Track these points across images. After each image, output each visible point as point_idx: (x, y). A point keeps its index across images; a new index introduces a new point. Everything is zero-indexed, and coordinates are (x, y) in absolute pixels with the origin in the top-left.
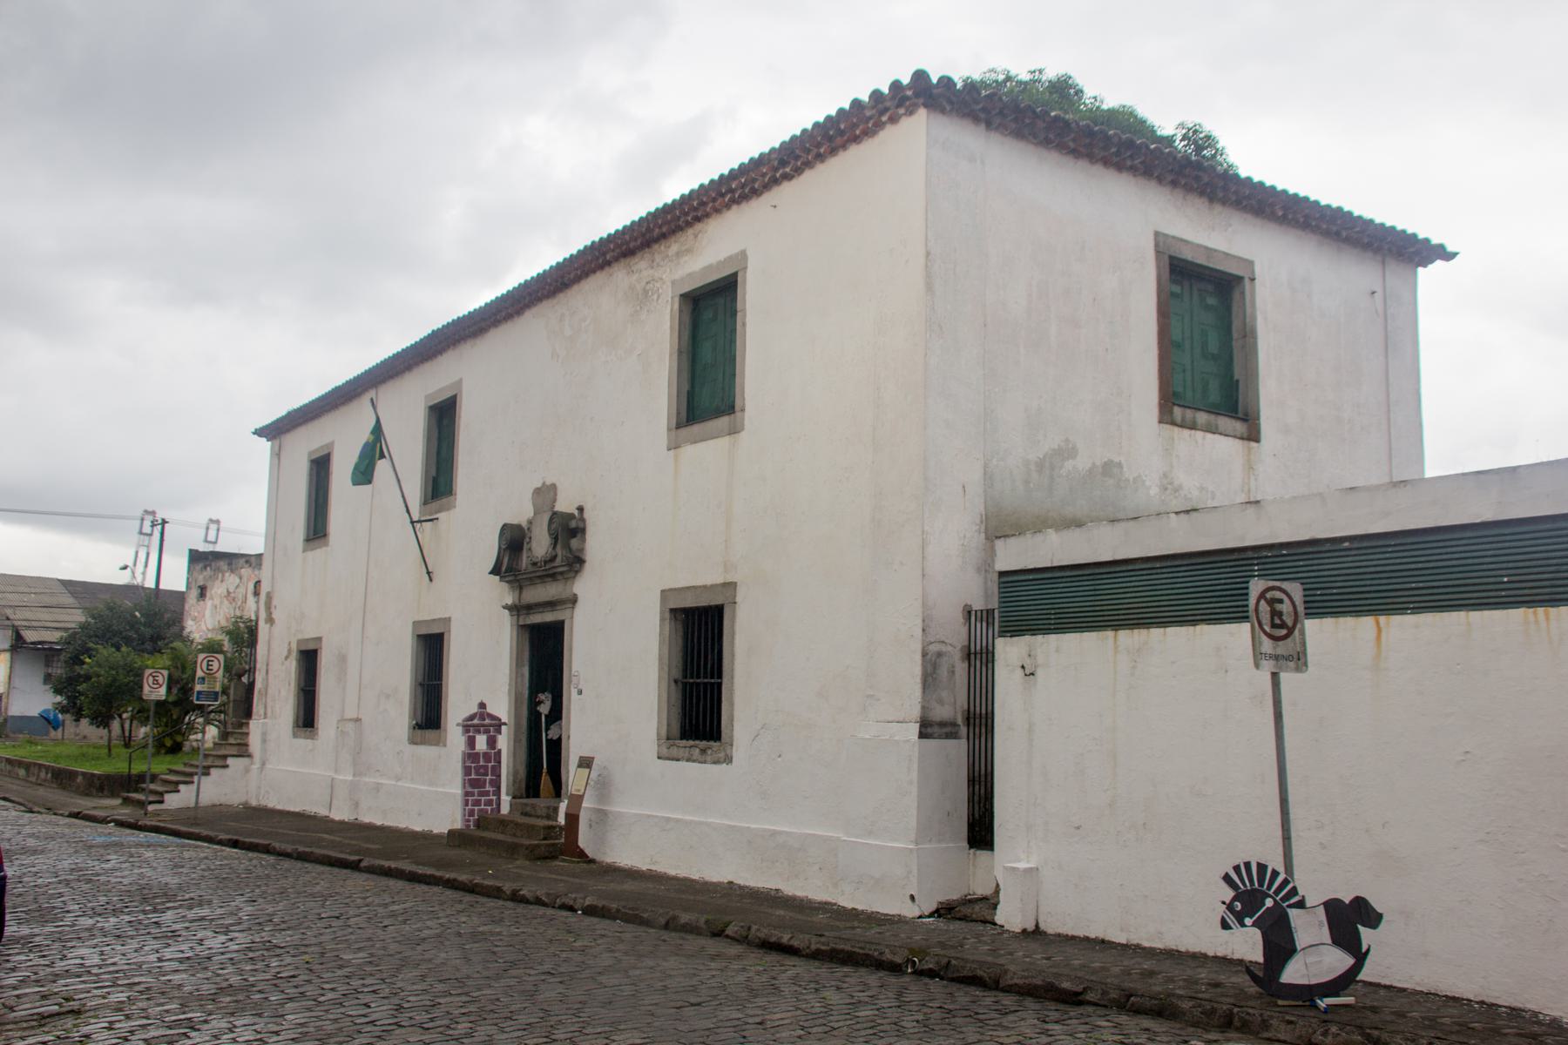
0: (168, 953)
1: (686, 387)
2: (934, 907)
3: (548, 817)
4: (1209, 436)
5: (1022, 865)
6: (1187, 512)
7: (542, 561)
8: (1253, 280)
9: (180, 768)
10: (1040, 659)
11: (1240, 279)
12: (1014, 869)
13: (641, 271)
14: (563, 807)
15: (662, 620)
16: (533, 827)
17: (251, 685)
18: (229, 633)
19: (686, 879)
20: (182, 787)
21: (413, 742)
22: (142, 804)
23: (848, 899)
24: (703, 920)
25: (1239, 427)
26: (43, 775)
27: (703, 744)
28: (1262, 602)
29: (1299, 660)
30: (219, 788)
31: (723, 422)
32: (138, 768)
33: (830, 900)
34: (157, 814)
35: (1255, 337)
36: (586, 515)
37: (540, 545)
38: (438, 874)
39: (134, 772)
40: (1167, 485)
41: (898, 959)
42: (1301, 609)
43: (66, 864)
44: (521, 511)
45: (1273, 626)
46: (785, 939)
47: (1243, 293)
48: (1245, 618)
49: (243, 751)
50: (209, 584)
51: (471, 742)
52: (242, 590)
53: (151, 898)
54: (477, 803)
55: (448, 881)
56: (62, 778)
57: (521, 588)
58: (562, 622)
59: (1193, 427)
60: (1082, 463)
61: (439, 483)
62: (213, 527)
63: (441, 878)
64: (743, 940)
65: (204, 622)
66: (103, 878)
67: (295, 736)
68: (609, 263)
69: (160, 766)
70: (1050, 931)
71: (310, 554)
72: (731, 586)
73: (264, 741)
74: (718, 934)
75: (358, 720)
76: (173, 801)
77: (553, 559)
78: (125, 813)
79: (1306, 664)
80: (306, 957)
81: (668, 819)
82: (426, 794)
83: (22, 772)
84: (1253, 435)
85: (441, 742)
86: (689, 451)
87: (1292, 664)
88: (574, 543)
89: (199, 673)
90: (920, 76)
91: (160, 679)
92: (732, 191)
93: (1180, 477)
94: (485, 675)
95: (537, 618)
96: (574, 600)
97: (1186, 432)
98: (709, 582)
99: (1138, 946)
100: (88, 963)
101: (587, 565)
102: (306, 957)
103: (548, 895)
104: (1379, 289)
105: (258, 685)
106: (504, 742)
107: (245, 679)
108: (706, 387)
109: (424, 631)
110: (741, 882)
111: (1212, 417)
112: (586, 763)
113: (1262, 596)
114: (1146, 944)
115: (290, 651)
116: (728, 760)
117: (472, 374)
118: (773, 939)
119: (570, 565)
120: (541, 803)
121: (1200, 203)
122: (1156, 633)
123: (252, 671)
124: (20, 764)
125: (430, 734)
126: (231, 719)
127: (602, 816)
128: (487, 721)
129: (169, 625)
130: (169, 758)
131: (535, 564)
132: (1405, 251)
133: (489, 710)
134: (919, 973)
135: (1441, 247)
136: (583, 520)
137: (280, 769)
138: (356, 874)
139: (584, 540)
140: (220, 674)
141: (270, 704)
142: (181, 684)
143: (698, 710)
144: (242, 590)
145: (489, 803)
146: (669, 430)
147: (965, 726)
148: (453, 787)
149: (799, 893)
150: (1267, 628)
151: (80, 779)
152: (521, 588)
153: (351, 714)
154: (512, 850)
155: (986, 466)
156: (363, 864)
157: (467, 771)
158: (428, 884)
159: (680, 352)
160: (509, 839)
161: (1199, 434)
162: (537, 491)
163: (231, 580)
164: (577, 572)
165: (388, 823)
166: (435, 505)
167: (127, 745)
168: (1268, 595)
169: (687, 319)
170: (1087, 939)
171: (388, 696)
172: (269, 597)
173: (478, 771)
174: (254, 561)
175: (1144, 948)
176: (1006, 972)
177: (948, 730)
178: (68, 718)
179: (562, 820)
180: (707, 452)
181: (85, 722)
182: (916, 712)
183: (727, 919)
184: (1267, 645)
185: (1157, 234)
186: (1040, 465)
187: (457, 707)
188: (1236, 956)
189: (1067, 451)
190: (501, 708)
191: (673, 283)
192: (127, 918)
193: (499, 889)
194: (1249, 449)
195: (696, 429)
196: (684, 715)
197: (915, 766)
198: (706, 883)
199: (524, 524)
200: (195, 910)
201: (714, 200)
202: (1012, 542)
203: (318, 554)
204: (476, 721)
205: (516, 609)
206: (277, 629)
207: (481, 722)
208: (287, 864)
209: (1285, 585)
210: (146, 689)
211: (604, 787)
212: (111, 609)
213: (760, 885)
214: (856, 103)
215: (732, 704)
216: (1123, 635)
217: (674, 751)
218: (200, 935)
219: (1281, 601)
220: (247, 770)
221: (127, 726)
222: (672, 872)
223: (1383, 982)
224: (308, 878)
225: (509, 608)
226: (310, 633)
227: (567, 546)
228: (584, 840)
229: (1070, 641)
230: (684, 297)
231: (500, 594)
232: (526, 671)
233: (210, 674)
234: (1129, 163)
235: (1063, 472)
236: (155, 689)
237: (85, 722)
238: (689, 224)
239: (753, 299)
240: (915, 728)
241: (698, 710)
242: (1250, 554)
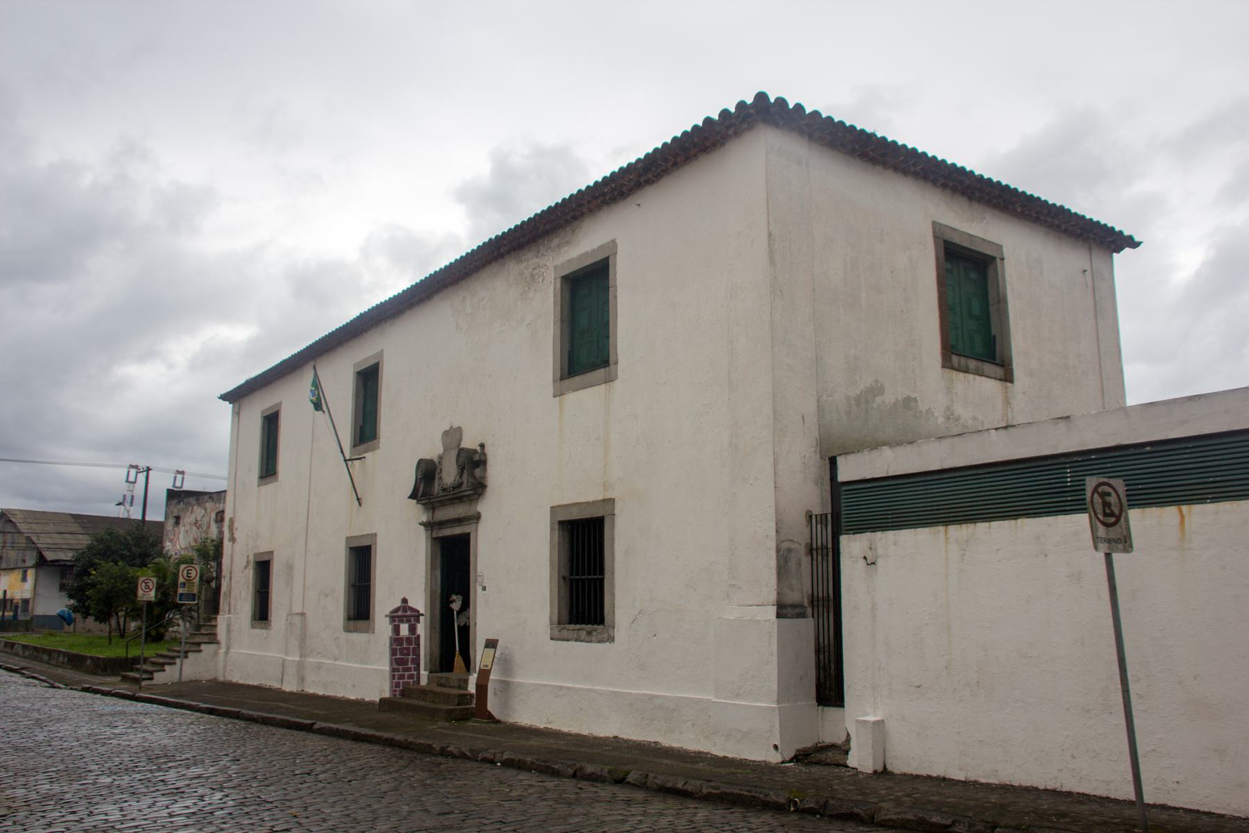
0: (176, 808)
1: (567, 348)
2: (792, 754)
3: (460, 687)
4: (978, 377)
5: (871, 718)
6: (1005, 428)
7: (452, 489)
8: (1003, 259)
9: (165, 652)
10: (880, 551)
11: (993, 259)
12: (865, 722)
13: (529, 262)
14: (473, 679)
15: (552, 530)
16: (449, 695)
17: (219, 587)
18: (198, 550)
19: (578, 736)
20: (167, 667)
21: (347, 630)
22: (136, 681)
23: (719, 749)
24: (606, 770)
25: (999, 371)
26: (61, 659)
28: (1096, 495)
29: (1125, 542)
30: (195, 667)
31: (601, 373)
32: (134, 652)
33: (702, 749)
34: (148, 688)
35: (1006, 302)
36: (487, 450)
37: (449, 475)
38: (378, 734)
39: (130, 656)
40: (950, 416)
41: (782, 801)
42: (1124, 500)
43: (84, 731)
44: (433, 449)
45: (1105, 515)
46: (680, 785)
48: (1084, 510)
49: (213, 639)
50: (182, 515)
51: (396, 630)
52: (206, 519)
53: (160, 758)
54: (402, 677)
55: (387, 740)
56: (76, 661)
58: (469, 534)
59: (966, 371)
60: (889, 398)
61: (366, 430)
62: (179, 477)
63: (348, 732)
64: (641, 786)
65: (179, 543)
66: (115, 742)
67: (253, 627)
69: (150, 651)
70: (896, 771)
71: (264, 488)
72: (610, 502)
73: (229, 631)
74: (620, 781)
75: (303, 614)
76: (159, 678)
77: (461, 485)
78: (124, 688)
79: (1131, 546)
80: (292, 811)
81: (561, 688)
82: (361, 670)
83: (45, 657)
84: (1008, 378)
85: (369, 630)
86: (572, 398)
87: (1121, 546)
88: (478, 472)
89: (181, 580)
90: (761, 97)
91: (150, 585)
92: (604, 194)
93: (960, 410)
94: (405, 576)
95: (448, 532)
96: (478, 517)
97: (962, 375)
98: (591, 499)
99: (975, 783)
100: (111, 818)
101: (489, 491)
102: (292, 811)
103: (471, 751)
104: (1087, 267)
105: (224, 589)
106: (421, 629)
107: (213, 584)
108: (586, 345)
109: (354, 544)
110: (625, 737)
111: (980, 364)
112: (491, 644)
113: (1095, 490)
114: (983, 780)
115: (248, 562)
116: (611, 639)
118: (669, 785)
120: (454, 676)
121: (963, 201)
122: (982, 527)
123: (219, 578)
124: (44, 651)
125: (361, 624)
126: (203, 615)
127: (506, 686)
128: (409, 613)
129: (153, 545)
130: (154, 645)
131: (444, 490)
132: (1109, 240)
133: (410, 604)
134: (804, 811)
135: (1131, 237)
136: (485, 454)
137: (243, 652)
138: (311, 736)
139: (485, 470)
140: (197, 580)
141: (233, 602)
142: (167, 590)
143: (584, 595)
144: (206, 519)
145: (411, 677)
146: (554, 381)
147: (816, 609)
148: (383, 665)
149: (675, 745)
150: (1100, 517)
151: (89, 662)
153: (297, 609)
154: (433, 714)
155: (818, 401)
156: (316, 727)
157: (393, 652)
158: (370, 742)
159: (562, 321)
160: (432, 706)
161: (971, 377)
162: (446, 433)
163: (199, 512)
165: (327, 694)
166: (362, 447)
167: (122, 636)
168: (1100, 490)
169: (567, 295)
170: (930, 777)
172: (232, 521)
173: (402, 652)
174: (219, 496)
175: (982, 784)
176: (880, 809)
177: (797, 611)
178: (78, 616)
179: (472, 689)
180: (587, 398)
181: (91, 619)
182: (773, 597)
183: (626, 768)
184: (1101, 529)
185: (934, 223)
186: (858, 399)
187: (383, 602)
188: (1065, 789)
189: (876, 390)
190: (419, 602)
191: (555, 268)
192: (138, 776)
193: (430, 746)
194: (1006, 391)
195: (577, 379)
196: (571, 605)
197: (775, 641)
198: (596, 738)
199: (436, 459)
200: (193, 769)
201: (589, 202)
202: (851, 457)
203: (270, 488)
205: (429, 526)
206: (237, 546)
207: (404, 613)
208: (255, 728)
209: (1112, 481)
210: (140, 592)
211: (507, 664)
212: (110, 534)
213: (641, 738)
214: (708, 121)
215: (613, 595)
216: (954, 530)
217: (565, 633)
218: (201, 791)
219: (1109, 494)
220: (216, 654)
221: (122, 620)
222: (565, 729)
223: (1202, 809)
224: (275, 739)
225: (422, 524)
226: (264, 548)
227: (472, 475)
228: (492, 705)
229: (906, 537)
230: (565, 279)
231: (416, 514)
232: (438, 573)
233: (189, 580)
234: (912, 169)
235: (875, 405)
236: (147, 592)
237: (91, 619)
238: (568, 222)
239: (623, 276)
240: (772, 611)
241: (584, 595)
242: (1062, 460)
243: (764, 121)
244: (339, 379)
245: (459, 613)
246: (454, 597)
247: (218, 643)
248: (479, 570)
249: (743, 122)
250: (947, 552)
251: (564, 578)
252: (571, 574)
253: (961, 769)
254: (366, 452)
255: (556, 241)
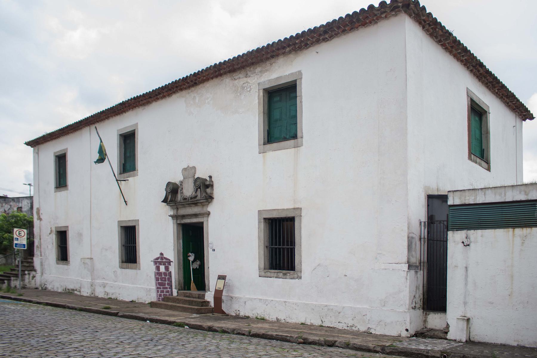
1: (267, 128)
10: (472, 239)
21: (121, 267)
25: (484, 164)
27: (284, 271)
31: (292, 142)
36: (213, 179)
44: (177, 178)
47: (487, 117)
51: (158, 268)
54: (162, 292)
57: (177, 209)
58: (202, 223)
59: (476, 163)
61: (128, 165)
68: (221, 75)
71: (59, 194)
77: (196, 197)
88: (208, 190)
96: (208, 214)
101: (215, 201)
106: (173, 269)
115: (51, 231)
116: (300, 278)
117: (142, 121)
119: (206, 199)
128: (164, 260)
131: (185, 199)
141: (42, 250)
145: (168, 292)
146: (259, 145)
152: (177, 209)
157: (157, 279)
162: (185, 170)
164: (209, 202)
166: (126, 175)
171: (106, 250)
172: (38, 210)
173: (162, 280)
182: (405, 259)
190: (171, 254)
191: (259, 84)
195: (275, 145)
199: (178, 183)
204: (159, 260)
205: (175, 217)
206: (43, 223)
207: (161, 260)
216: (518, 231)
217: (269, 274)
229: (489, 233)
231: (167, 211)
232: (181, 241)
238: (267, 59)
243: (405, 12)
244: (110, 134)
245: (193, 262)
246: (190, 254)
247: (35, 271)
248: (210, 240)
249: (392, 11)
250: (513, 241)
251: (267, 247)
252: (272, 245)
253: (515, 341)
254: (129, 177)
255: (258, 69)
